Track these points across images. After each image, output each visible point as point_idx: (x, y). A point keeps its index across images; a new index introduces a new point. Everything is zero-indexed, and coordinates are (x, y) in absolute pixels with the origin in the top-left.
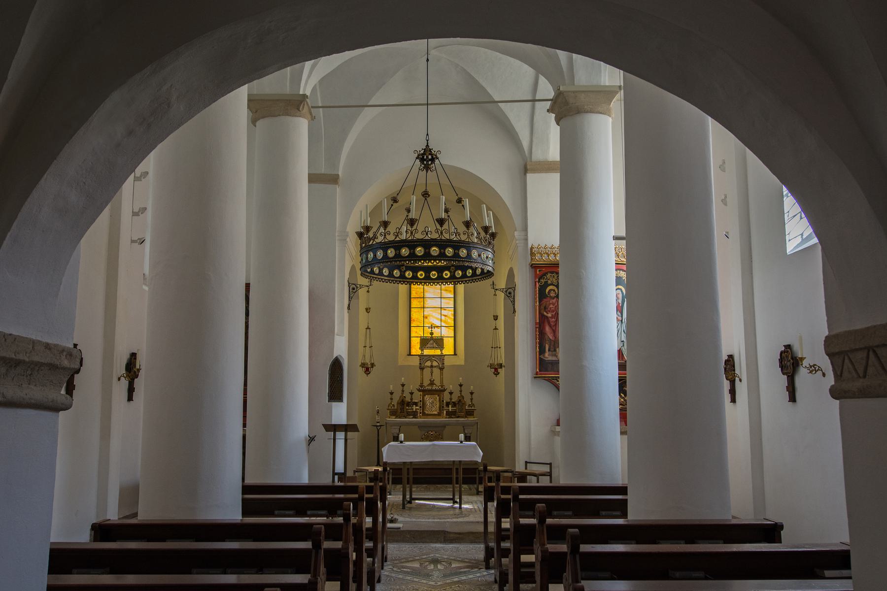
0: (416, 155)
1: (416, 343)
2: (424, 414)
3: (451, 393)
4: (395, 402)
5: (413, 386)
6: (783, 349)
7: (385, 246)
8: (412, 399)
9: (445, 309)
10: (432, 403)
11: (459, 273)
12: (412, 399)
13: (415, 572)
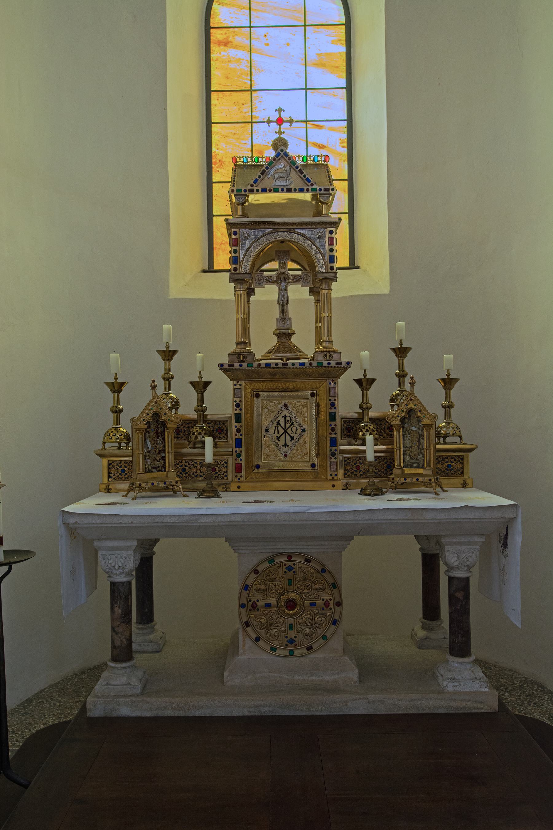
3: (365, 384)
5: (206, 354)
9: (317, 124)
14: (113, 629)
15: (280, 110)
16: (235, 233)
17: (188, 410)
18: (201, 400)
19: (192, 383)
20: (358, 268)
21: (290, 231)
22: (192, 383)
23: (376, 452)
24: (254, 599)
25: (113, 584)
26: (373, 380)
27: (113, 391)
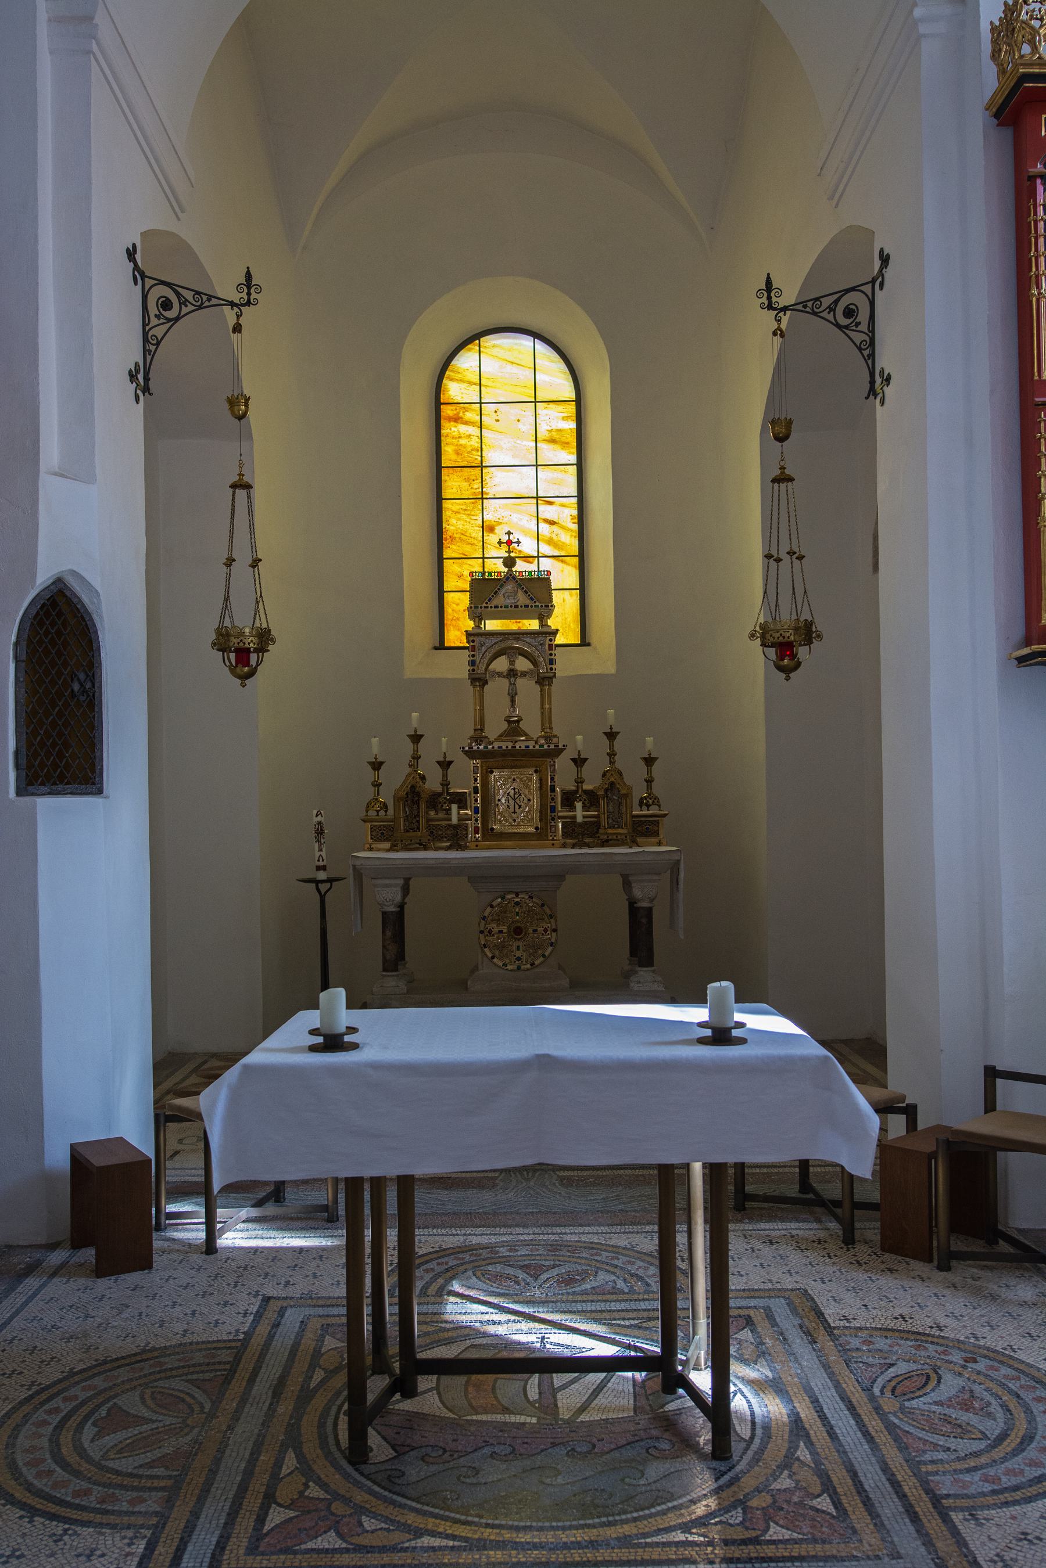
1: (458, 603)
2: (488, 833)
3: (579, 762)
4: (386, 796)
5: (448, 739)
8: (446, 784)
10: (514, 796)
12: (446, 784)
14: (384, 947)
15: (509, 533)
16: (473, 641)
17: (433, 784)
18: (445, 775)
19: (438, 762)
20: (589, 645)
21: (518, 640)
22: (438, 762)
23: (584, 817)
24: (489, 927)
25: (384, 914)
26: (586, 759)
27: (374, 769)
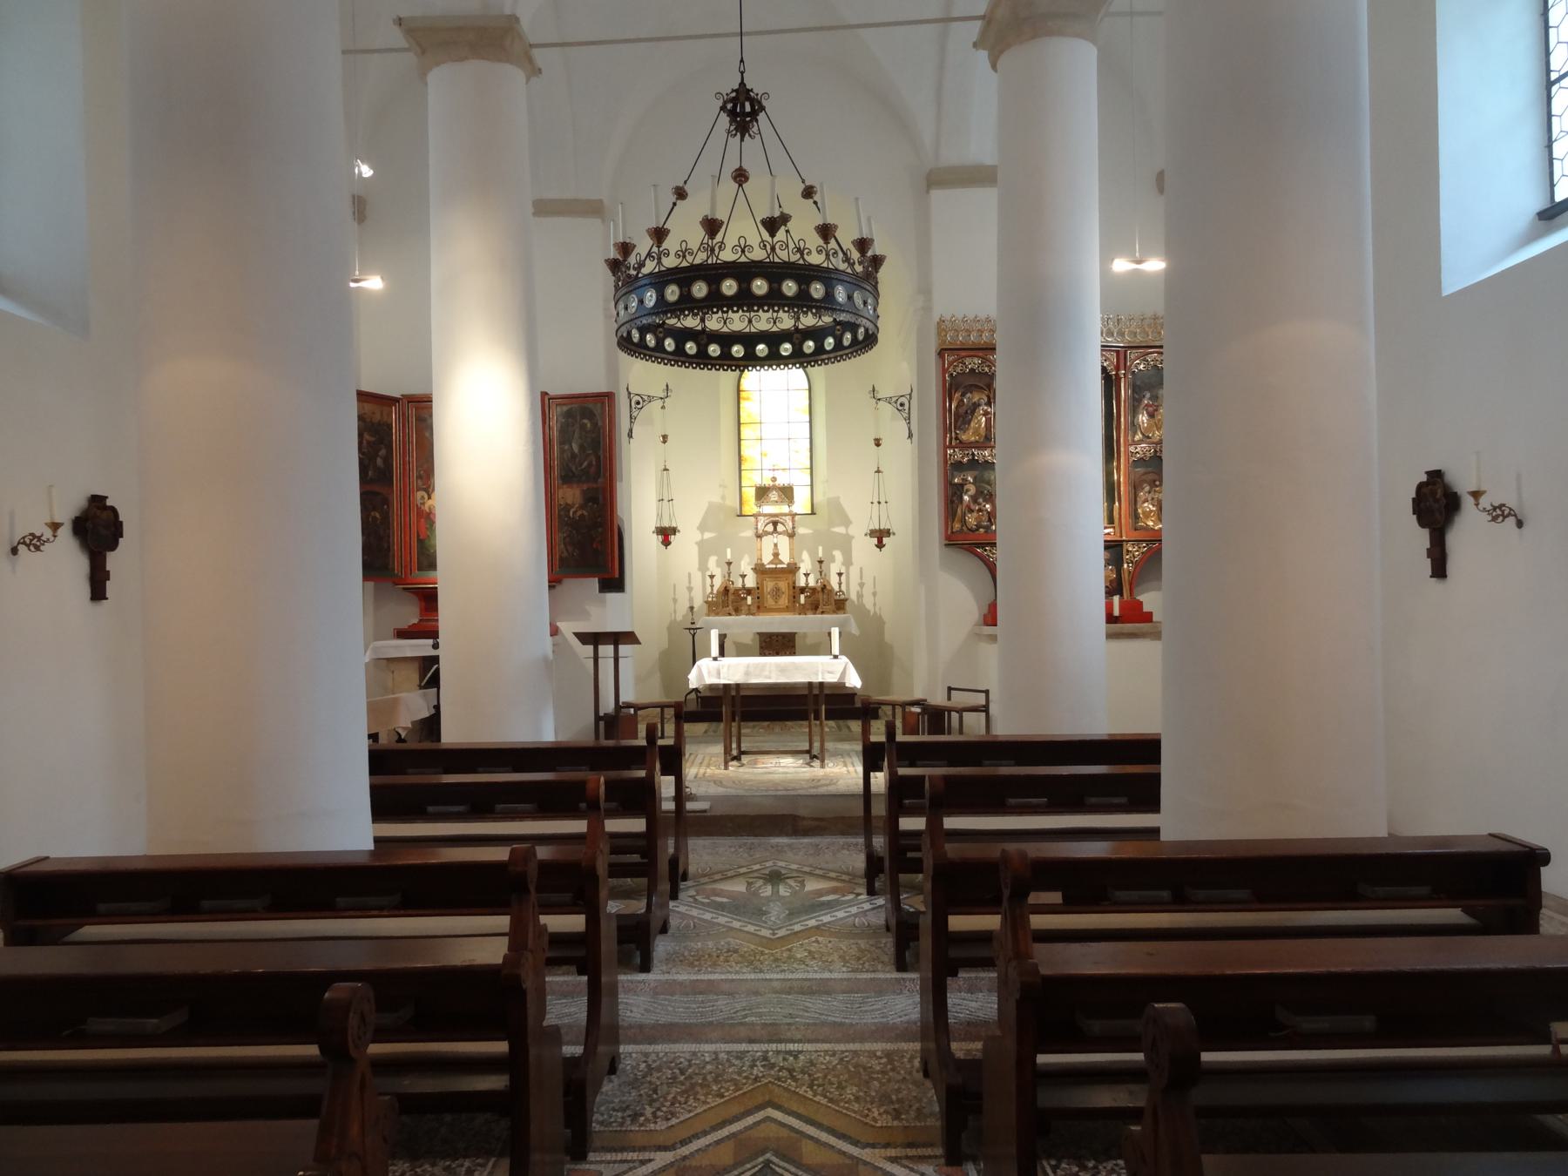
0: (720, 103)
6: (1424, 478)
7: (660, 280)
11: (809, 346)
13: (737, 907)
